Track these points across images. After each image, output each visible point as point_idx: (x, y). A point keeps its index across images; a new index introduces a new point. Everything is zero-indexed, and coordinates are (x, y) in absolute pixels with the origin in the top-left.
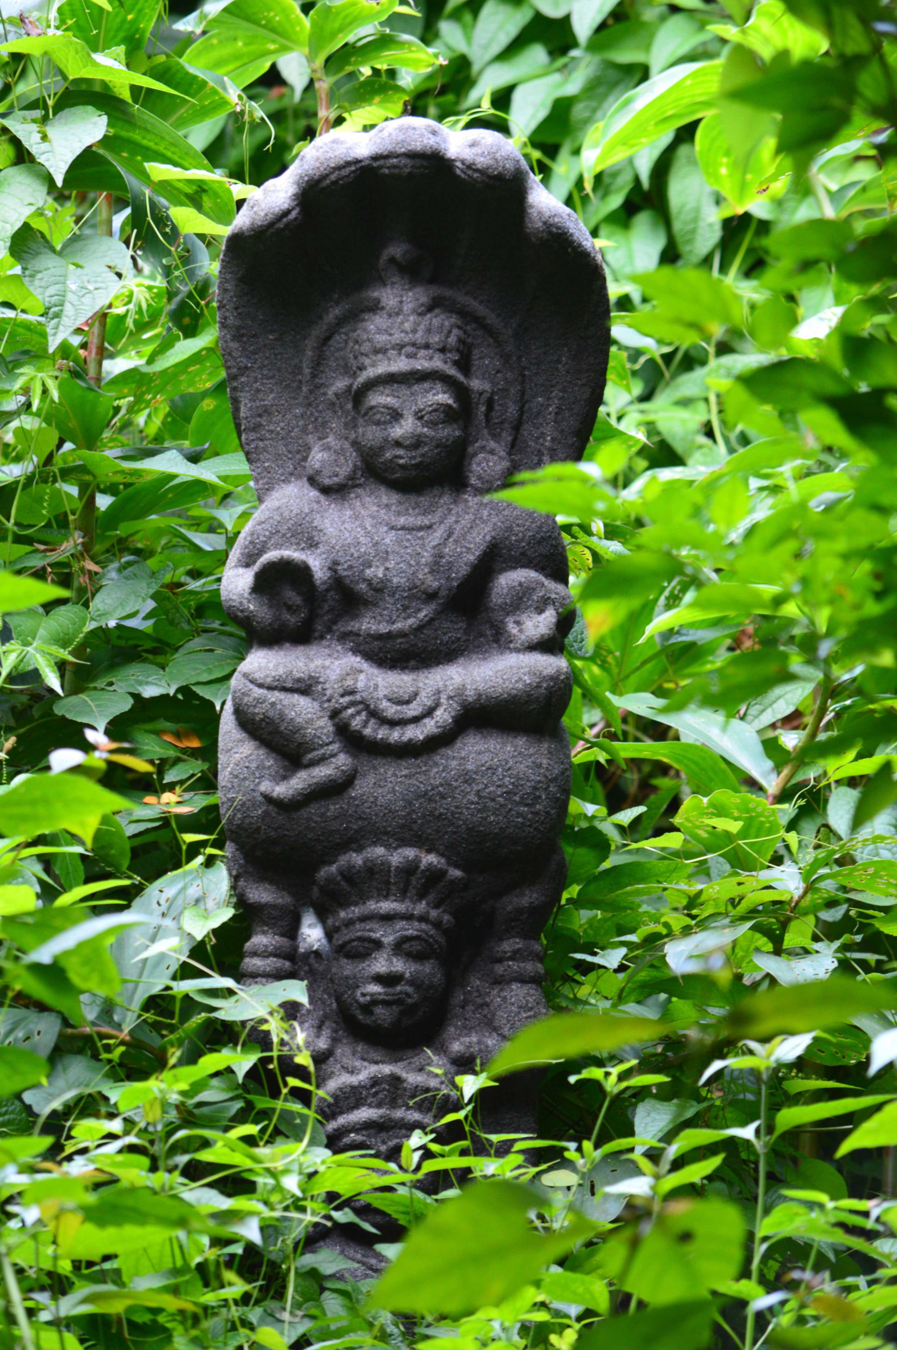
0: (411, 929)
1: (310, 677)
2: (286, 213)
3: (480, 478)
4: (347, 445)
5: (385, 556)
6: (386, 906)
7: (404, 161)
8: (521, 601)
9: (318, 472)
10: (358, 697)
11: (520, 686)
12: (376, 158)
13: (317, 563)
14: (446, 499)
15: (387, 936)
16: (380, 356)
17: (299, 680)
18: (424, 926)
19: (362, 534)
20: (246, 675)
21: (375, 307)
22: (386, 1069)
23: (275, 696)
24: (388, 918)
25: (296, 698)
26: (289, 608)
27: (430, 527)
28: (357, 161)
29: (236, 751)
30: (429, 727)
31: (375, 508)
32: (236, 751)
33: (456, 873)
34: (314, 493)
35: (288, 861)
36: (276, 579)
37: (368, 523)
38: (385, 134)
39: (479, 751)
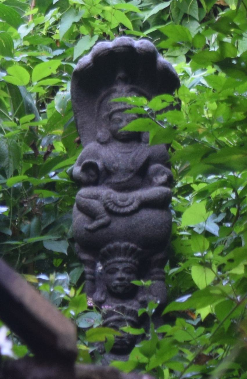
0: (127, 265)
1: (98, 195)
2: (89, 64)
3: (145, 139)
4: (107, 131)
5: (118, 160)
6: (120, 259)
7: (122, 48)
8: (157, 172)
9: (100, 138)
10: (111, 200)
11: (157, 196)
12: (114, 47)
13: (99, 163)
14: (135, 145)
15: (120, 267)
16: (116, 105)
17: (95, 196)
18: (131, 264)
20: (80, 195)
21: (115, 91)
22: (121, 305)
23: (88, 200)
24: (121, 262)
25: (94, 200)
26: (92, 176)
27: (131, 152)
28: (109, 49)
29: (78, 217)
30: (132, 207)
31: (115, 148)
33: (139, 249)
34: (98, 144)
36: (88, 167)
37: (114, 152)
38: (117, 41)
39: (146, 214)
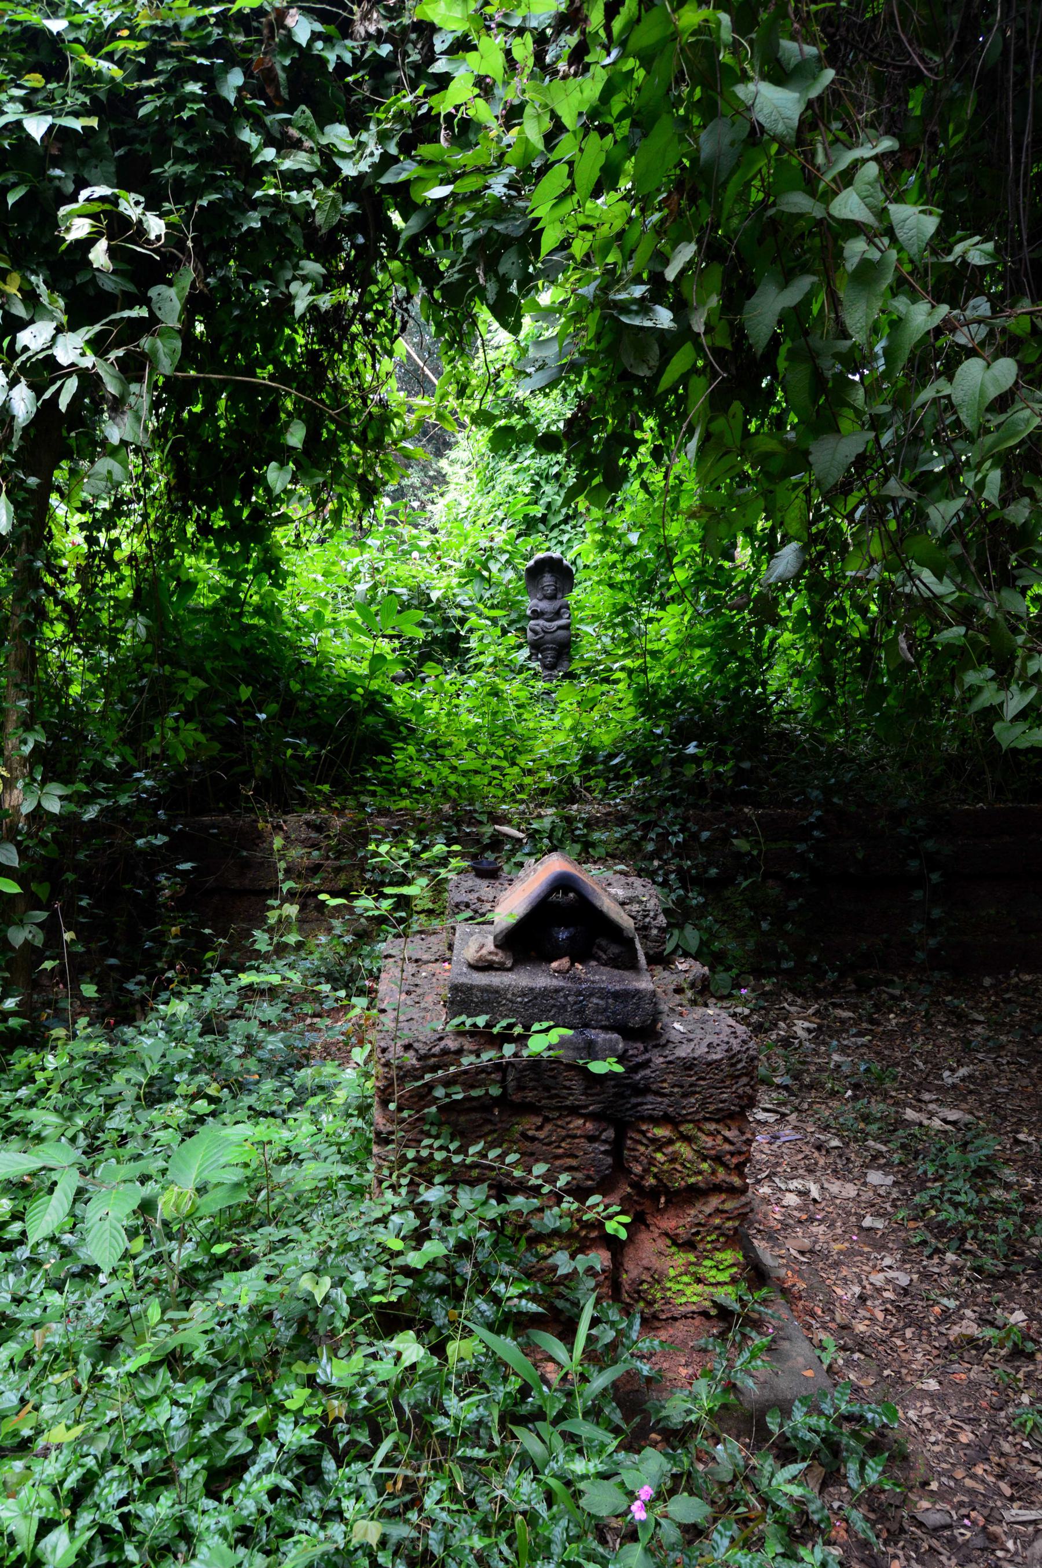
19: (544, 605)
29: (529, 633)
32: (529, 633)
35: (536, 647)
39: (560, 632)
